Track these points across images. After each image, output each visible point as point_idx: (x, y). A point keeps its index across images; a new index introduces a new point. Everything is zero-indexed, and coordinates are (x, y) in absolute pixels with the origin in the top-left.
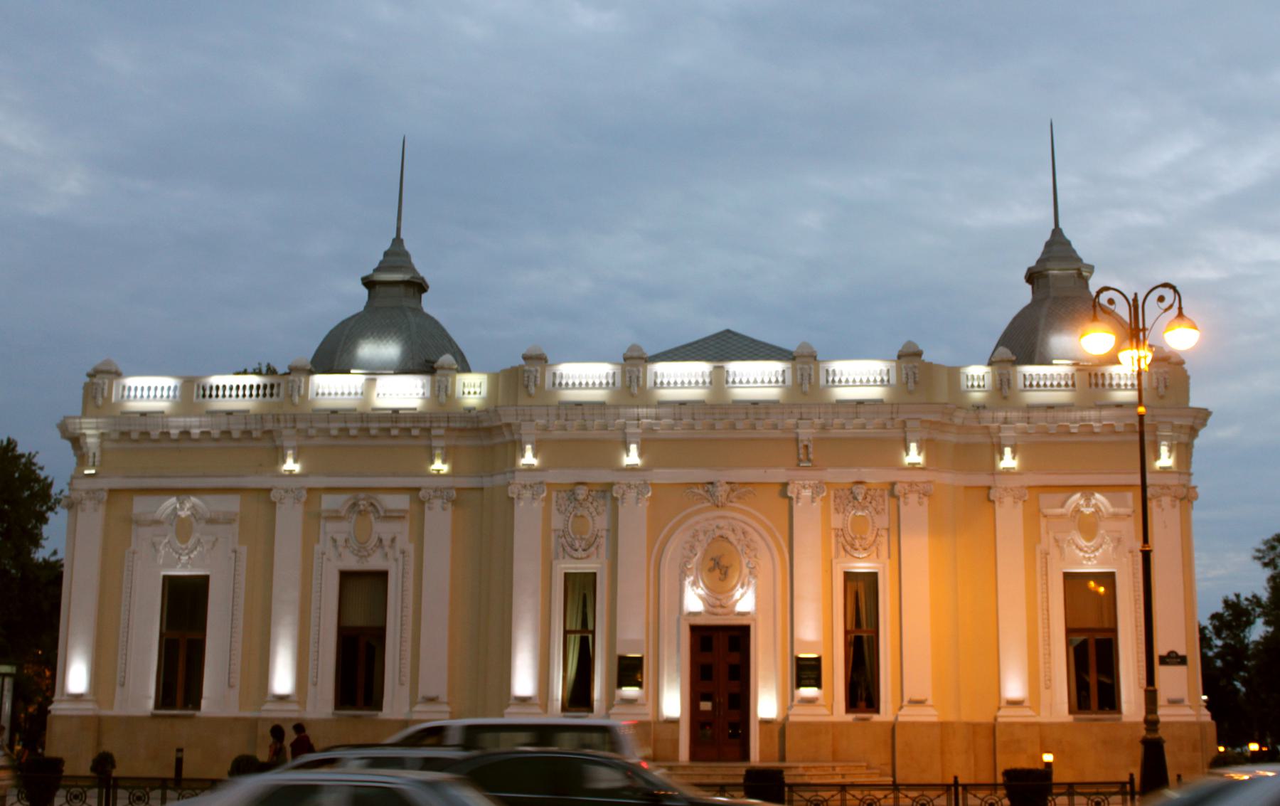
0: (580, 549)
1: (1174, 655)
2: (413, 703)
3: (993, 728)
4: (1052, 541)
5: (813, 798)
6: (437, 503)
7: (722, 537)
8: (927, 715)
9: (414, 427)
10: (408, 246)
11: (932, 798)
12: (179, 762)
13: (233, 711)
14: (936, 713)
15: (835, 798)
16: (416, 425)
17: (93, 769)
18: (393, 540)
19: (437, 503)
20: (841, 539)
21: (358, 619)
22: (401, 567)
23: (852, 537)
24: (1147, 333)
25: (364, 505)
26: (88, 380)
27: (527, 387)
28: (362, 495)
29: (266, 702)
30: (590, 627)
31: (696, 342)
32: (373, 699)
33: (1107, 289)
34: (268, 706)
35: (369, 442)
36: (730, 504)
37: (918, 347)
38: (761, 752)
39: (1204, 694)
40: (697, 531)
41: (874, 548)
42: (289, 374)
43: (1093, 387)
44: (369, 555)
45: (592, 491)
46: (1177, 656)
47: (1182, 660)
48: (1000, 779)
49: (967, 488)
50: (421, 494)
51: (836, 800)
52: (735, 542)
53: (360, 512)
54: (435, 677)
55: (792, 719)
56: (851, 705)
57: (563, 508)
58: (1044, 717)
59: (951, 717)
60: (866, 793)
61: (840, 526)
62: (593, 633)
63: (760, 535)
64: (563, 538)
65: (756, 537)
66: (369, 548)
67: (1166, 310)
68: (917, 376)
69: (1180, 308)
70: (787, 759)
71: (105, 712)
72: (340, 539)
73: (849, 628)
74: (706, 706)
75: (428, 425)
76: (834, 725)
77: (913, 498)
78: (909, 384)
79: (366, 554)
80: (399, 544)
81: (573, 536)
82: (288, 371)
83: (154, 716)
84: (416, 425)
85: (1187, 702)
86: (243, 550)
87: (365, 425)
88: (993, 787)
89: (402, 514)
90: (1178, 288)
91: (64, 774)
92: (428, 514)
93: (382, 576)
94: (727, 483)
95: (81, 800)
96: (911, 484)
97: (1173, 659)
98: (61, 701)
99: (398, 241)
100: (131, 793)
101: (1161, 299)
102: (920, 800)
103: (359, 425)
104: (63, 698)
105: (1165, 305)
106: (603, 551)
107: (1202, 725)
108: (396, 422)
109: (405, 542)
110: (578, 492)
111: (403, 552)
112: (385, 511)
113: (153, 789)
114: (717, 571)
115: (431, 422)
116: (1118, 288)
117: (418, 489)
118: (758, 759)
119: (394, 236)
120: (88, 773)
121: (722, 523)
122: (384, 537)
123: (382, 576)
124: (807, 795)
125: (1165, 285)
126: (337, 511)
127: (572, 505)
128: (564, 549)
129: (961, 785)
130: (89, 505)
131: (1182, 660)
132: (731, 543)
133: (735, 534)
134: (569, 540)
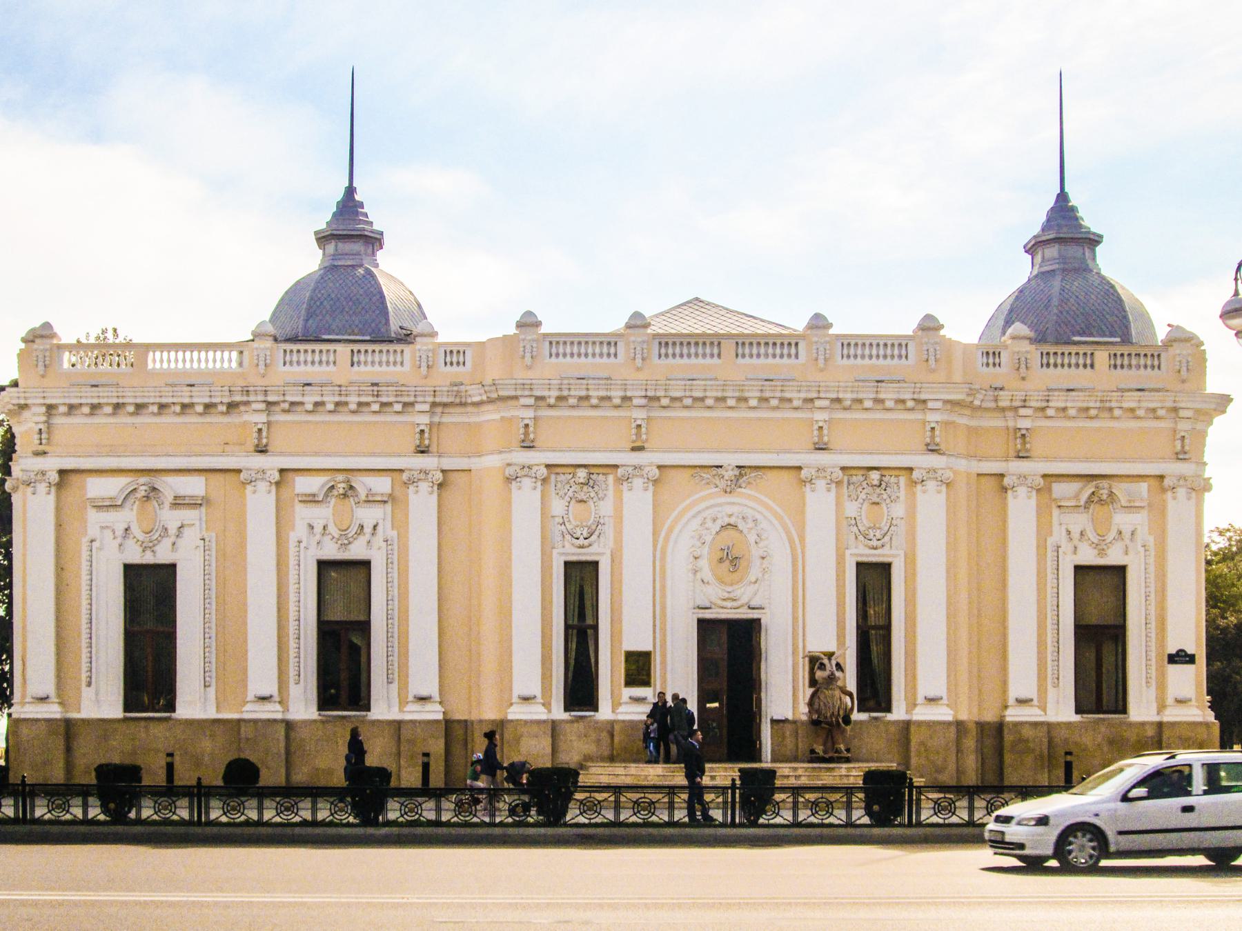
0: (874, 539)
2: (1162, 707)
3: (999, 728)
4: (1064, 533)
6: (1022, 491)
8: (943, 714)
10: (1074, 201)
12: (170, 767)
13: (211, 713)
16: (399, 399)
17: (225, 778)
19: (1022, 491)
21: (337, 614)
26: (23, 346)
30: (589, 621)
34: (248, 707)
35: (1069, 424)
36: (739, 490)
38: (773, 751)
39: (1208, 695)
41: (887, 538)
42: (253, 340)
44: (350, 543)
45: (885, 476)
46: (1187, 655)
47: (1191, 659)
54: (424, 679)
55: (1008, 719)
56: (326, 701)
59: (963, 716)
62: (595, 628)
64: (855, 528)
66: (350, 535)
68: (938, 352)
71: (74, 715)
75: (412, 399)
78: (637, 361)
79: (346, 542)
82: (252, 338)
84: (399, 399)
85: (1035, 702)
93: (1121, 571)
94: (737, 467)
95: (950, 811)
97: (1181, 657)
98: (23, 704)
99: (1062, 197)
100: (224, 803)
102: (996, 801)
107: (1207, 725)
108: (377, 396)
115: (415, 396)
119: (347, 185)
120: (220, 783)
121: (735, 509)
122: (1122, 528)
123: (1121, 571)
126: (314, 495)
129: (917, 787)
131: (1191, 659)
133: (747, 523)
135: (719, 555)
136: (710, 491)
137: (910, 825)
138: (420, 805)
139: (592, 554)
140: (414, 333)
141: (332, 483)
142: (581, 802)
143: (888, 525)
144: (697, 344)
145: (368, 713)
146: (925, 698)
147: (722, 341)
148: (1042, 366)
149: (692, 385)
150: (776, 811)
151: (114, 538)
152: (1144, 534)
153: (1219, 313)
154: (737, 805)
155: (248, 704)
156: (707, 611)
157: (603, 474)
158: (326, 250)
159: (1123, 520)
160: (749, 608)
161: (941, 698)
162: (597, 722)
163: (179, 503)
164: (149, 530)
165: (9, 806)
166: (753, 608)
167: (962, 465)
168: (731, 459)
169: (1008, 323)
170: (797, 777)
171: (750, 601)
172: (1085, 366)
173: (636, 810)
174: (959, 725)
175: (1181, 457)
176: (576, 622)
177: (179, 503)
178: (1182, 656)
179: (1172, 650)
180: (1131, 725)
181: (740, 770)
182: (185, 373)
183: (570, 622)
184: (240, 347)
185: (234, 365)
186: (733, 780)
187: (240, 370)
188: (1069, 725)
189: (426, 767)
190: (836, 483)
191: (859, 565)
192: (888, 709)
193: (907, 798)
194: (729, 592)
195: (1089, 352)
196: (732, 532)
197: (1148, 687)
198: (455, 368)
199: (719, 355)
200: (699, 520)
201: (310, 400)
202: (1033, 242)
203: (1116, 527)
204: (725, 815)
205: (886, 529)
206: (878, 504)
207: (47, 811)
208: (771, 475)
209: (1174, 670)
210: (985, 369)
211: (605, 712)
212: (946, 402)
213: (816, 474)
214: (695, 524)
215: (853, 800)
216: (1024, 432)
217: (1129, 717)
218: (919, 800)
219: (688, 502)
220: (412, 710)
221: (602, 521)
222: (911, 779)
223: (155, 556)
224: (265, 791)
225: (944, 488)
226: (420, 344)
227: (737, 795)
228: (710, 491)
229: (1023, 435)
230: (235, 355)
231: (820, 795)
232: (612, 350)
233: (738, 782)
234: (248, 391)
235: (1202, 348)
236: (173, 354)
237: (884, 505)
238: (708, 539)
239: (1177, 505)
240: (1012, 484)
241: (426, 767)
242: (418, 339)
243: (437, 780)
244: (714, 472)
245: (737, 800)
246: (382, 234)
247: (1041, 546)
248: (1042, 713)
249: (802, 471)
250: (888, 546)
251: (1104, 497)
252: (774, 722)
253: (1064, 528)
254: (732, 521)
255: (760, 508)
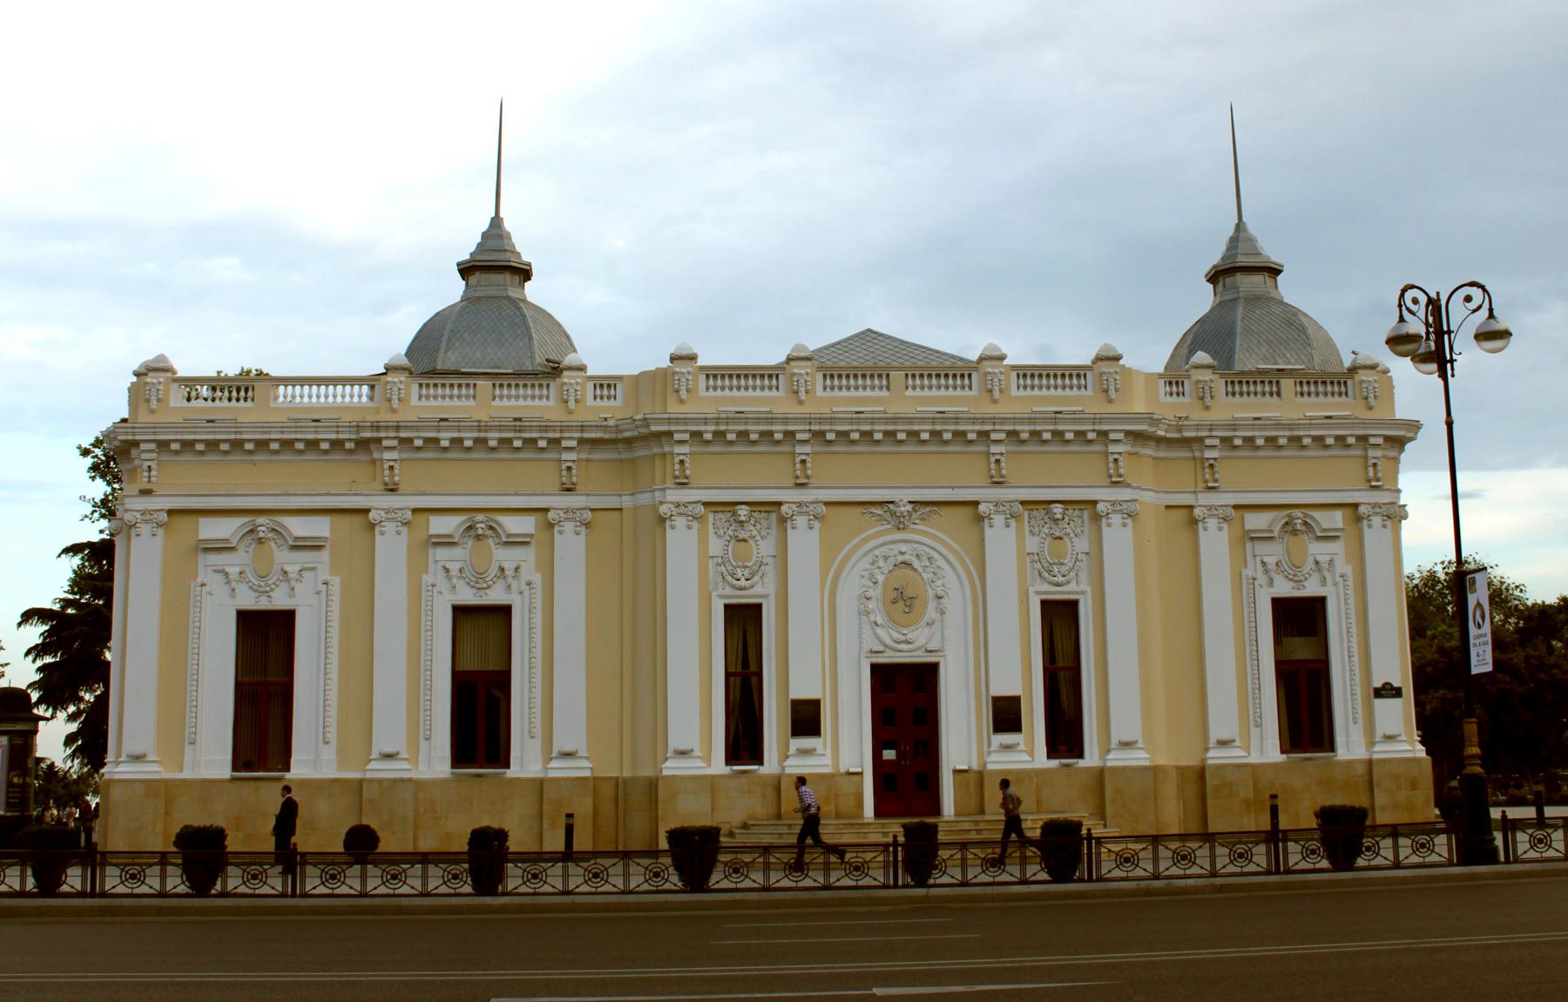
0: (743, 579)
1: (1389, 687)
2: (1371, 743)
3: (1201, 773)
5: (852, 860)
6: (1212, 523)
7: (905, 563)
8: (1138, 758)
9: (542, 438)
10: (508, 225)
11: (607, 866)
12: (1274, 811)
14: (1147, 756)
15: (877, 859)
18: (517, 569)
19: (569, 527)
20: (1038, 565)
22: (527, 602)
23: (734, 566)
24: (1453, 335)
25: (482, 529)
26: (134, 379)
27: (677, 391)
28: (480, 517)
29: (370, 761)
30: (753, 668)
31: (838, 343)
32: (498, 755)
33: (1413, 287)
34: (372, 765)
37: (1001, 351)
40: (877, 556)
41: (1073, 574)
43: (598, 399)
46: (1393, 688)
47: (1397, 693)
48: (663, 844)
49: (1168, 507)
50: (551, 515)
51: (878, 862)
52: (920, 570)
53: (478, 537)
54: (572, 731)
55: (990, 767)
57: (722, 531)
58: (1255, 758)
59: (1161, 761)
60: (990, 850)
61: (1036, 551)
63: (949, 562)
64: (723, 567)
65: (941, 562)
67: (1475, 311)
69: (1491, 310)
70: (987, 812)
72: (454, 568)
73: (732, 669)
74: (889, 755)
75: (558, 435)
76: (1039, 773)
77: (1116, 519)
79: (485, 585)
80: (525, 575)
81: (734, 564)
82: (385, 371)
83: (233, 779)
84: (1237, 434)
86: (336, 581)
87: (482, 435)
88: (163, 859)
89: (528, 540)
90: (1487, 288)
91: (228, 850)
92: (988, 532)
93: (505, 611)
94: (910, 502)
96: (800, 504)
97: (1388, 691)
98: (118, 763)
99: (496, 221)
101: (1468, 299)
103: (713, 428)
104: (121, 759)
105: (1473, 305)
106: (1473, 575)
109: (531, 573)
110: (740, 512)
111: (529, 584)
112: (509, 536)
113: (1257, 843)
114: (901, 603)
116: (1453, 289)
117: (546, 510)
118: (952, 813)
120: (342, 850)
122: (506, 565)
123: (505, 611)
124: (1115, 848)
125: (1472, 284)
126: (450, 536)
127: (732, 528)
128: (1040, 574)
129: (1096, 838)
130: (145, 529)
131: (1397, 693)
132: (916, 570)
134: (729, 568)
135: (894, 594)
136: (883, 527)
137: (1090, 880)
138: (545, 870)
139: (1069, 593)
140: (561, 366)
141: (469, 524)
142: (726, 864)
143: (1073, 560)
144: (1048, 376)
145: (507, 770)
146: (1120, 742)
147: (891, 373)
148: (1227, 394)
149: (858, 418)
150: (1249, 858)
151: (1256, 579)
152: (1344, 567)
153: (1385, 339)
154: (900, 864)
155: (372, 762)
156: (880, 655)
157: (766, 512)
158: (469, 282)
159: (1319, 550)
160: (927, 651)
161: (1234, 741)
162: (762, 776)
163: (300, 545)
164: (266, 574)
165: (1015, 864)
166: (931, 651)
167: (1147, 497)
168: (904, 496)
169: (1191, 352)
170: (979, 831)
171: (927, 643)
172: (1271, 394)
173: (848, 872)
174: (1155, 771)
175: (1373, 484)
176: (739, 669)
177: (300, 545)
178: (1388, 690)
179: (1378, 684)
180: (1339, 763)
181: (904, 826)
182: (310, 409)
183: (730, 670)
184: (372, 382)
185: (364, 399)
186: (895, 837)
187: (371, 405)
188: (1275, 766)
189: (569, 830)
190: (586, 524)
191: (1043, 603)
192: (1080, 755)
193: (1085, 852)
194: (903, 634)
195: (1274, 380)
196: (908, 571)
197: (1355, 723)
198: (605, 403)
199: (888, 388)
200: (869, 558)
201: (445, 438)
202: (1213, 272)
203: (1312, 558)
204: (285, 885)
205: (1071, 565)
206: (1060, 538)
207: (521, 882)
208: (945, 511)
209: (1379, 703)
210: (1169, 399)
211: (771, 764)
212: (1128, 433)
213: (995, 508)
214: (865, 563)
215: (968, 857)
216: (1211, 462)
217: (1336, 756)
218: (1099, 854)
219: (857, 539)
220: (374, 768)
221: (765, 561)
222: (1089, 830)
223: (270, 602)
224: (430, 857)
225: (583, 529)
226: (567, 377)
227: (900, 853)
228: (883, 527)
229: (1211, 466)
230: (365, 388)
231: (1124, 846)
232: (774, 382)
233: (901, 839)
234: (378, 426)
235: (1389, 374)
236: (348, 388)
237: (751, 542)
238: (880, 578)
239: (1374, 534)
240: (379, 519)
241: (569, 830)
242: (565, 373)
243: (582, 843)
244: (886, 508)
245: (900, 858)
246: (529, 265)
247: (1237, 578)
248: (1030, 759)
249: (370, 514)
250: (1075, 581)
251: (1299, 527)
252: (956, 772)
253: (1258, 559)
254: (906, 558)
255: (937, 546)
